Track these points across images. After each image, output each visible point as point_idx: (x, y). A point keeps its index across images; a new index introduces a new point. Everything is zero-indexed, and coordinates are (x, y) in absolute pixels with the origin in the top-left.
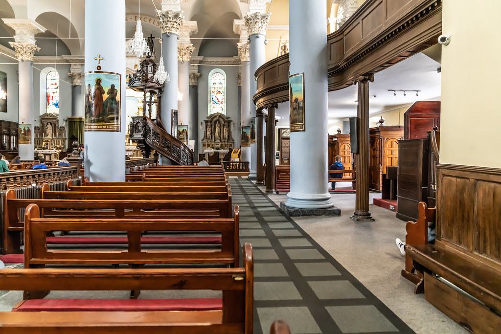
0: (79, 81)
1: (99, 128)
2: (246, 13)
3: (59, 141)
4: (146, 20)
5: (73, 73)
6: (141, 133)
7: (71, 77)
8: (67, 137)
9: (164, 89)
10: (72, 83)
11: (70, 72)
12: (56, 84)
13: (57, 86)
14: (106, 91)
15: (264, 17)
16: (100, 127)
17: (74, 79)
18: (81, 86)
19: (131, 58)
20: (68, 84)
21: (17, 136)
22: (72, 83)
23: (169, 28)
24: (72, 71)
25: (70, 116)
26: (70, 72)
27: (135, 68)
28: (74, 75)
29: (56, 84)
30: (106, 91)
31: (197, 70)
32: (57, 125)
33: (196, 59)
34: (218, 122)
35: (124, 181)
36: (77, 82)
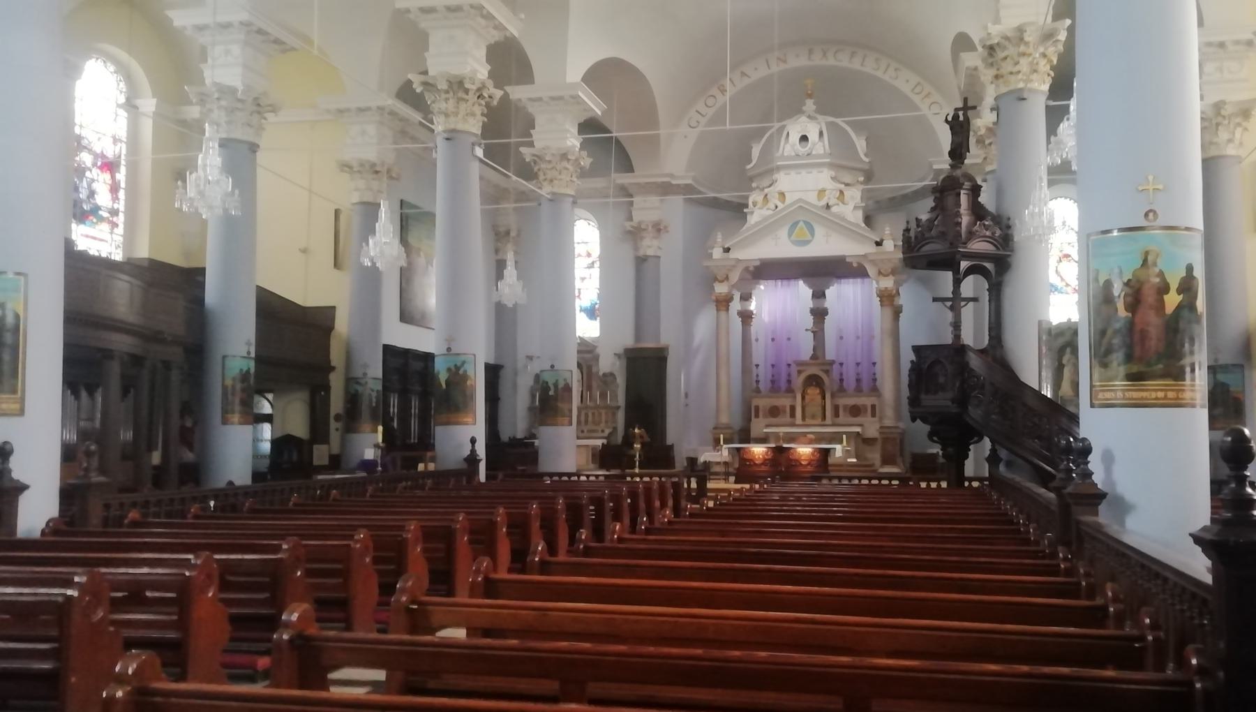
0: (655, 243)
1: (1157, 399)
2: (986, 28)
3: (600, 414)
5: (640, 223)
6: (950, 395)
7: (634, 234)
8: (621, 400)
10: (636, 249)
12: (589, 255)
13: (590, 260)
14: (1174, 285)
16: (1160, 394)
17: (642, 238)
18: (659, 257)
20: (626, 254)
21: (425, 396)
22: (636, 249)
24: (637, 216)
25: (629, 342)
26: (630, 218)
28: (643, 227)
29: (589, 255)
30: (1174, 285)
32: (594, 370)
34: (1068, 350)
36: (649, 246)
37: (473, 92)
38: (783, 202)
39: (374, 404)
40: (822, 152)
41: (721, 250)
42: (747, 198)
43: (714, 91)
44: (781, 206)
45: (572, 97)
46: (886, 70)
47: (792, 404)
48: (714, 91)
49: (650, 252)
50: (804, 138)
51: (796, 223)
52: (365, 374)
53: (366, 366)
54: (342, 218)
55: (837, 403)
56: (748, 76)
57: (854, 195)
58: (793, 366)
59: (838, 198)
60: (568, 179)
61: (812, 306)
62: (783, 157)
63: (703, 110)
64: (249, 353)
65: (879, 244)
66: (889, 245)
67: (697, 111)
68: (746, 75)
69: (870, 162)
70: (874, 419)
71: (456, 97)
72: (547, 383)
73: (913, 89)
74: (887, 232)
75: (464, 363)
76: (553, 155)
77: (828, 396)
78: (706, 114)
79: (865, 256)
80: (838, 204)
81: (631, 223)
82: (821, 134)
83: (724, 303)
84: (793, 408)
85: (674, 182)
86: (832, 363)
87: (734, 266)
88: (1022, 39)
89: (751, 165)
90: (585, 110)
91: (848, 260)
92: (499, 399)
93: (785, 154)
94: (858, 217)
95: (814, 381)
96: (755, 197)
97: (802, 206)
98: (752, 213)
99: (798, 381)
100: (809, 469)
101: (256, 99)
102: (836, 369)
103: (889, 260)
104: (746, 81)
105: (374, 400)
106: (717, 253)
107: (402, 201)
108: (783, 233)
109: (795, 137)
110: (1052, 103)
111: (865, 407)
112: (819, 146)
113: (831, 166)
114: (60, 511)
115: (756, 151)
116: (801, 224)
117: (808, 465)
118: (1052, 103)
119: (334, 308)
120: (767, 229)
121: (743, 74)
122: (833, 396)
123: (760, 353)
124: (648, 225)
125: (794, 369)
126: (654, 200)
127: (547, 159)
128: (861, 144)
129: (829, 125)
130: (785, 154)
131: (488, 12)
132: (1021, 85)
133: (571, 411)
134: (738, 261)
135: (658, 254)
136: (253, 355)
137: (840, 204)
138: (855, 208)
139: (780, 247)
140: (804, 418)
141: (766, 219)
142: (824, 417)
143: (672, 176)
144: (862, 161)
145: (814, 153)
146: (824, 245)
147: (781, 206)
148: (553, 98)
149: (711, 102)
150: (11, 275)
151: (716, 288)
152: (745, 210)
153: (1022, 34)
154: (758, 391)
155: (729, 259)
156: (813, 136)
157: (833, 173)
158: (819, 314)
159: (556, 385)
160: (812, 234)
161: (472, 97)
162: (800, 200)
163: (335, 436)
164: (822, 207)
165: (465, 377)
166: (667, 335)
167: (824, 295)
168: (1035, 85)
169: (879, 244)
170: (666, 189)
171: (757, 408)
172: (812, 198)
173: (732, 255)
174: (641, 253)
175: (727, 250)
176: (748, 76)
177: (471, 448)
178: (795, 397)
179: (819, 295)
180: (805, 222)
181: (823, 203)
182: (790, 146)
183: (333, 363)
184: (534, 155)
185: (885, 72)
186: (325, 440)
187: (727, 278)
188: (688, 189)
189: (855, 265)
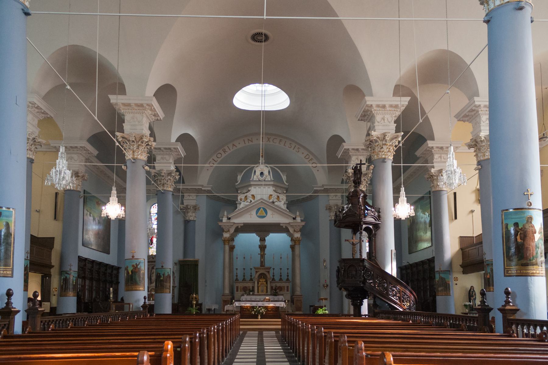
0: (194, 214)
4: (275, 141)
5: (187, 206)
9: (378, 232)
11: (183, 204)
15: (35, 141)
17: (188, 212)
18: (195, 221)
19: (267, 187)
23: (385, 152)
24: (186, 203)
25: (181, 258)
26: (182, 203)
27: (269, 200)
31: (341, 201)
33: (339, 187)
35: (171, 313)
36: (191, 216)
37: (145, 142)
38: (254, 199)
39: (74, 284)
40: (270, 180)
41: (226, 218)
42: (237, 196)
43: (221, 151)
44: (253, 201)
45: (174, 148)
46: (294, 148)
47: (253, 285)
48: (221, 151)
49: (192, 218)
50: (262, 174)
51: (259, 209)
52: (70, 269)
53: (71, 265)
54: (59, 197)
55: (272, 285)
56: (236, 146)
57: (283, 197)
58: (253, 269)
59: (277, 199)
60: (171, 184)
61: (260, 244)
62: (253, 181)
63: (216, 159)
64: (27, 257)
65: (294, 219)
66: (298, 219)
67: (213, 159)
68: (235, 145)
69: (288, 185)
70: (288, 292)
71: (137, 144)
72: (160, 274)
73: (305, 157)
74: (297, 214)
75: (140, 263)
76: (165, 173)
77: (269, 282)
78: (217, 161)
79: (289, 223)
80: (277, 202)
81: (183, 206)
82: (269, 172)
83: (227, 241)
84: (253, 287)
85: (203, 189)
86: (270, 268)
87: (232, 226)
88: (384, 138)
89: (238, 183)
90: (178, 155)
91: (281, 225)
92: (119, 282)
93: (254, 180)
94: (284, 207)
95: (262, 276)
96: (241, 196)
97: (262, 201)
98: (240, 203)
99: (255, 276)
100: (272, 312)
101: (34, 139)
102: (271, 271)
103: (299, 226)
104: (235, 148)
105: (74, 281)
106: (225, 220)
107: (84, 190)
108: (254, 212)
109: (258, 173)
110: (394, 164)
111: (284, 287)
112: (268, 177)
113: (273, 185)
114: (50, 310)
115: (239, 178)
116: (262, 209)
117: (271, 310)
118: (394, 164)
119: (54, 238)
120: (247, 210)
121: (234, 145)
122: (271, 282)
123: (238, 264)
124: (191, 207)
125: (253, 271)
126: (193, 196)
127: (162, 175)
128: (284, 178)
129: (271, 167)
130: (254, 180)
131: (154, 108)
132: (384, 156)
133: (170, 286)
134: (234, 223)
135: (195, 219)
136: (29, 258)
137: (278, 202)
138: (284, 203)
139: (252, 218)
140: (258, 292)
141: (247, 206)
142: (267, 292)
143: (202, 186)
144: (285, 184)
145: (266, 180)
146: (271, 218)
147: (253, 201)
148: (166, 149)
149: (219, 156)
150: (4, 209)
151: (224, 235)
152: (236, 202)
153: (385, 136)
154: (237, 280)
155: (230, 222)
156: (266, 173)
157: (274, 189)
158: (263, 248)
159: (164, 275)
160: (266, 214)
161: (144, 145)
162: (262, 199)
163: (54, 299)
164: (271, 202)
165: (139, 270)
166: (199, 254)
167: (265, 240)
168: (390, 157)
169: (294, 219)
170: (199, 191)
171: (237, 287)
172: (266, 197)
173: (232, 221)
174: (187, 218)
175: (229, 219)
176: (236, 146)
177: (144, 301)
178: (254, 283)
179: (263, 240)
180: (263, 208)
181: (271, 201)
182: (256, 177)
183: (53, 264)
184: (155, 173)
185: (293, 149)
186: (49, 300)
187: (229, 231)
188: (209, 191)
189: (284, 227)
